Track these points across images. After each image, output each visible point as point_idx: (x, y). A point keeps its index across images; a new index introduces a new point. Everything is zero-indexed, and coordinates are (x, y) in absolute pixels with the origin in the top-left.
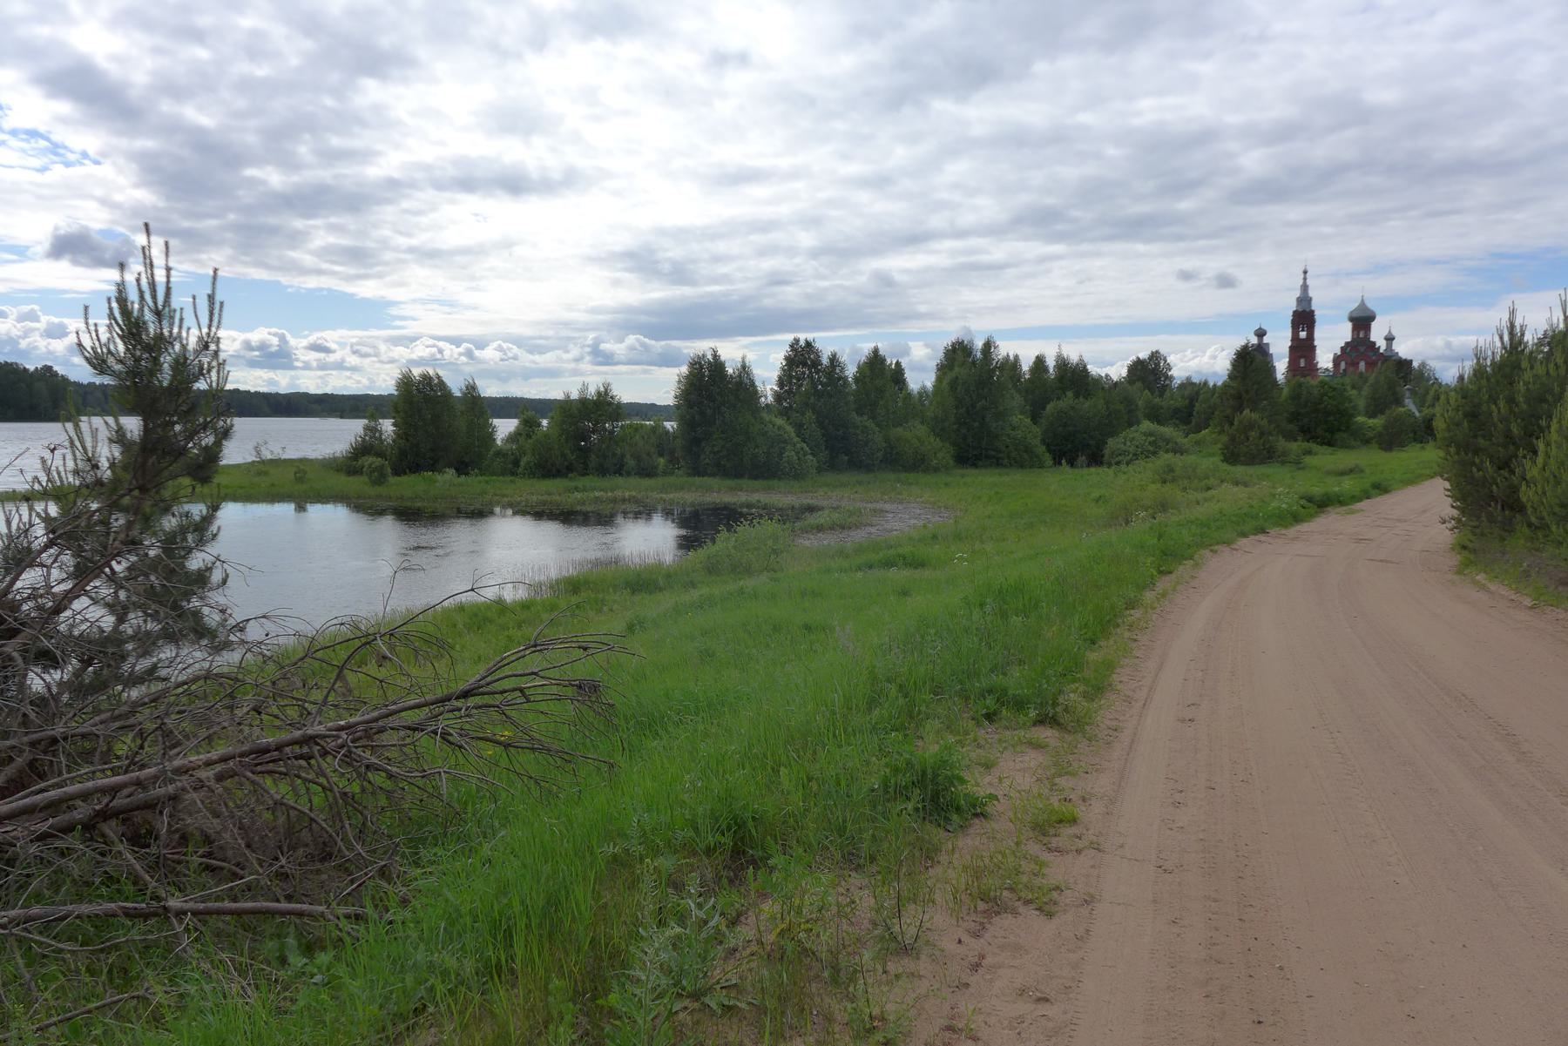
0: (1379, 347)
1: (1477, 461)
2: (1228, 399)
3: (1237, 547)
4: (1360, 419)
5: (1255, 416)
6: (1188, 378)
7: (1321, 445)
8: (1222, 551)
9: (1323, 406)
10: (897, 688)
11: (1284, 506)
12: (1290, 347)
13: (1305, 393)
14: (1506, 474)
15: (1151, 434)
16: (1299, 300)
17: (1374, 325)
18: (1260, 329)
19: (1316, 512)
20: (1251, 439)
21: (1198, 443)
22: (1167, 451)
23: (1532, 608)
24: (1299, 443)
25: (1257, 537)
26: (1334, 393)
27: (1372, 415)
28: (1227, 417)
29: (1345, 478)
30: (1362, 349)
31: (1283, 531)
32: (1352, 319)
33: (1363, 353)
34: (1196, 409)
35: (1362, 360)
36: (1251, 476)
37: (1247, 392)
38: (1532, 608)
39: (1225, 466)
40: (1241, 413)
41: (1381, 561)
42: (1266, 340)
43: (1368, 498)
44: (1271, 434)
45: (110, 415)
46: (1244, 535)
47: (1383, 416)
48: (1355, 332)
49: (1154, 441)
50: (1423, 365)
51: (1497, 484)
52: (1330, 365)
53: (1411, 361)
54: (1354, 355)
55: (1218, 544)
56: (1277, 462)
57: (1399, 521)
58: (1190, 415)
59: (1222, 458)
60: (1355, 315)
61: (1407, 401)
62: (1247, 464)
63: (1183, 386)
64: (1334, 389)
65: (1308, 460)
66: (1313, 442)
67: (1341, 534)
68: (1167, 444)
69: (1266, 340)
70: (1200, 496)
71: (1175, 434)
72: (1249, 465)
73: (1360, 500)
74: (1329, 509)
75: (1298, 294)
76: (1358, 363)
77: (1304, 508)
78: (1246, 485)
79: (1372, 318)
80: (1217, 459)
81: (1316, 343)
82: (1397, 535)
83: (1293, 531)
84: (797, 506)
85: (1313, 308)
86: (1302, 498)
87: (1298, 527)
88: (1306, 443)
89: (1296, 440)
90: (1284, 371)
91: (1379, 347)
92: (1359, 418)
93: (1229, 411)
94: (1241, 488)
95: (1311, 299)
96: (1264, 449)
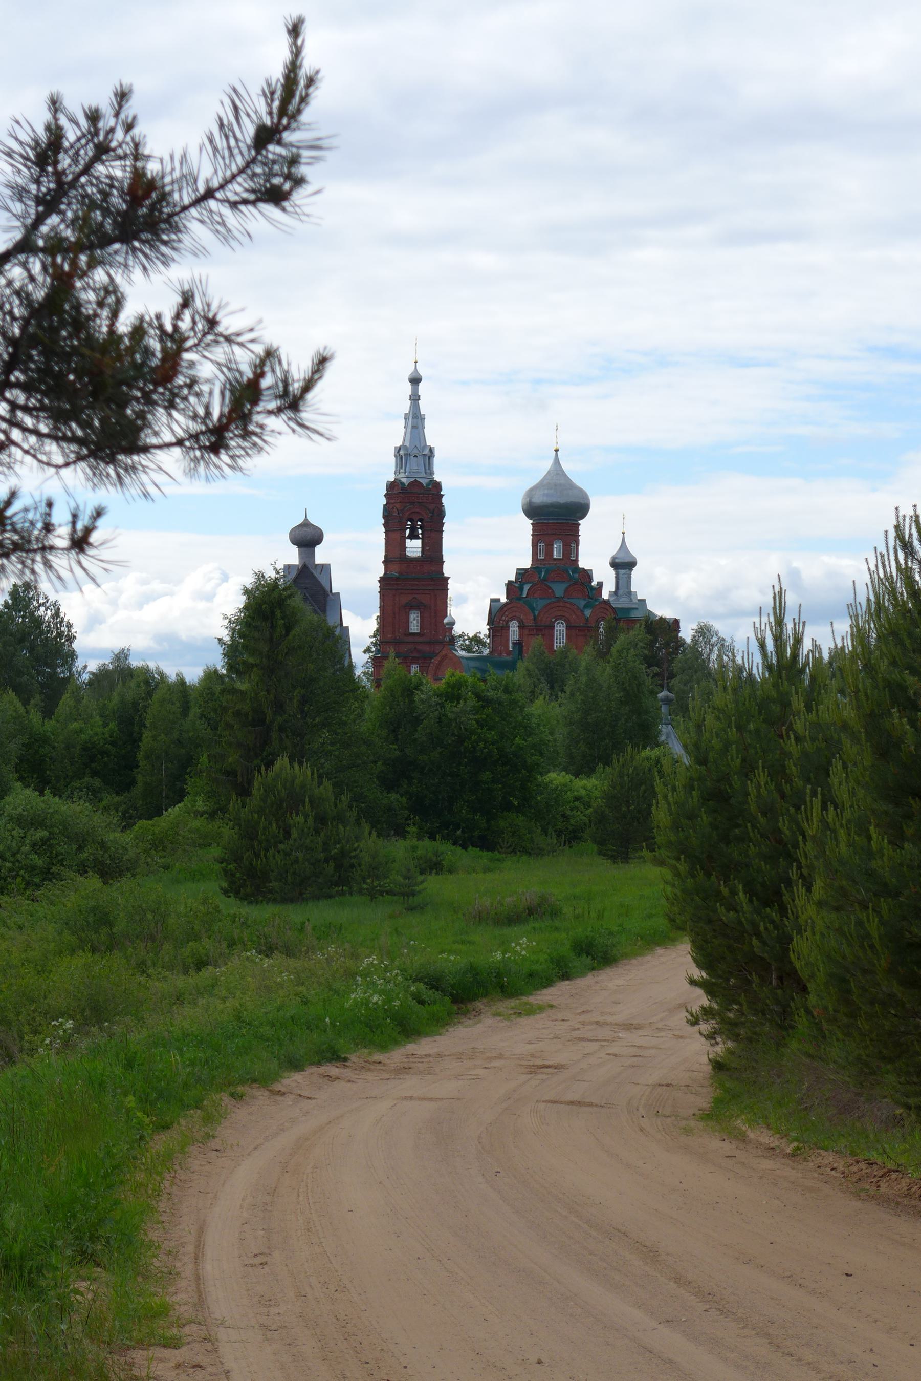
0: (600, 584)
1: (725, 891)
2: (229, 726)
3: (283, 1090)
4: (556, 778)
5: (302, 773)
6: (121, 656)
8: (254, 1098)
10: (521, 745)
11: (375, 998)
12: (382, 580)
14: (775, 916)
15: (37, 822)
16: (403, 456)
17: (586, 527)
18: (306, 524)
19: (449, 1014)
20: (295, 834)
21: (158, 844)
22: (83, 870)
23: (792, 1155)
24: (408, 843)
25: (322, 1070)
27: (583, 768)
28: (230, 773)
29: (516, 930)
30: (559, 589)
31: (377, 1057)
32: (531, 511)
33: (559, 599)
35: (512, 619)
36: (302, 929)
37: (279, 707)
38: (792, 1155)
39: (231, 906)
40: (269, 764)
41: (572, 1103)
42: (321, 555)
46: (295, 1065)
47: (608, 769)
48: (541, 545)
49: (44, 841)
50: (704, 632)
51: (758, 935)
52: (482, 629)
53: (676, 622)
54: (540, 604)
55: (242, 1082)
56: (361, 892)
57: (629, 1027)
58: (129, 763)
59: (225, 885)
60: (539, 499)
61: (665, 729)
62: (286, 900)
63: (102, 678)
65: (432, 884)
66: (445, 838)
67: (500, 1057)
68: (80, 848)
69: (321, 555)
70: (181, 982)
71: (99, 819)
72: (292, 901)
73: (548, 983)
74: (479, 1004)
75: (397, 435)
76: (552, 628)
77: (421, 1002)
78: (289, 952)
79: (580, 509)
80: (212, 887)
82: (615, 1055)
83: (396, 1056)
84: (496, 852)
85: (437, 477)
86: (417, 979)
87: (411, 1048)
88: (427, 842)
89: (401, 832)
90: (369, 641)
91: (600, 584)
92: (552, 775)
93: (233, 758)
94: (278, 958)
95: (430, 454)
96: (326, 861)
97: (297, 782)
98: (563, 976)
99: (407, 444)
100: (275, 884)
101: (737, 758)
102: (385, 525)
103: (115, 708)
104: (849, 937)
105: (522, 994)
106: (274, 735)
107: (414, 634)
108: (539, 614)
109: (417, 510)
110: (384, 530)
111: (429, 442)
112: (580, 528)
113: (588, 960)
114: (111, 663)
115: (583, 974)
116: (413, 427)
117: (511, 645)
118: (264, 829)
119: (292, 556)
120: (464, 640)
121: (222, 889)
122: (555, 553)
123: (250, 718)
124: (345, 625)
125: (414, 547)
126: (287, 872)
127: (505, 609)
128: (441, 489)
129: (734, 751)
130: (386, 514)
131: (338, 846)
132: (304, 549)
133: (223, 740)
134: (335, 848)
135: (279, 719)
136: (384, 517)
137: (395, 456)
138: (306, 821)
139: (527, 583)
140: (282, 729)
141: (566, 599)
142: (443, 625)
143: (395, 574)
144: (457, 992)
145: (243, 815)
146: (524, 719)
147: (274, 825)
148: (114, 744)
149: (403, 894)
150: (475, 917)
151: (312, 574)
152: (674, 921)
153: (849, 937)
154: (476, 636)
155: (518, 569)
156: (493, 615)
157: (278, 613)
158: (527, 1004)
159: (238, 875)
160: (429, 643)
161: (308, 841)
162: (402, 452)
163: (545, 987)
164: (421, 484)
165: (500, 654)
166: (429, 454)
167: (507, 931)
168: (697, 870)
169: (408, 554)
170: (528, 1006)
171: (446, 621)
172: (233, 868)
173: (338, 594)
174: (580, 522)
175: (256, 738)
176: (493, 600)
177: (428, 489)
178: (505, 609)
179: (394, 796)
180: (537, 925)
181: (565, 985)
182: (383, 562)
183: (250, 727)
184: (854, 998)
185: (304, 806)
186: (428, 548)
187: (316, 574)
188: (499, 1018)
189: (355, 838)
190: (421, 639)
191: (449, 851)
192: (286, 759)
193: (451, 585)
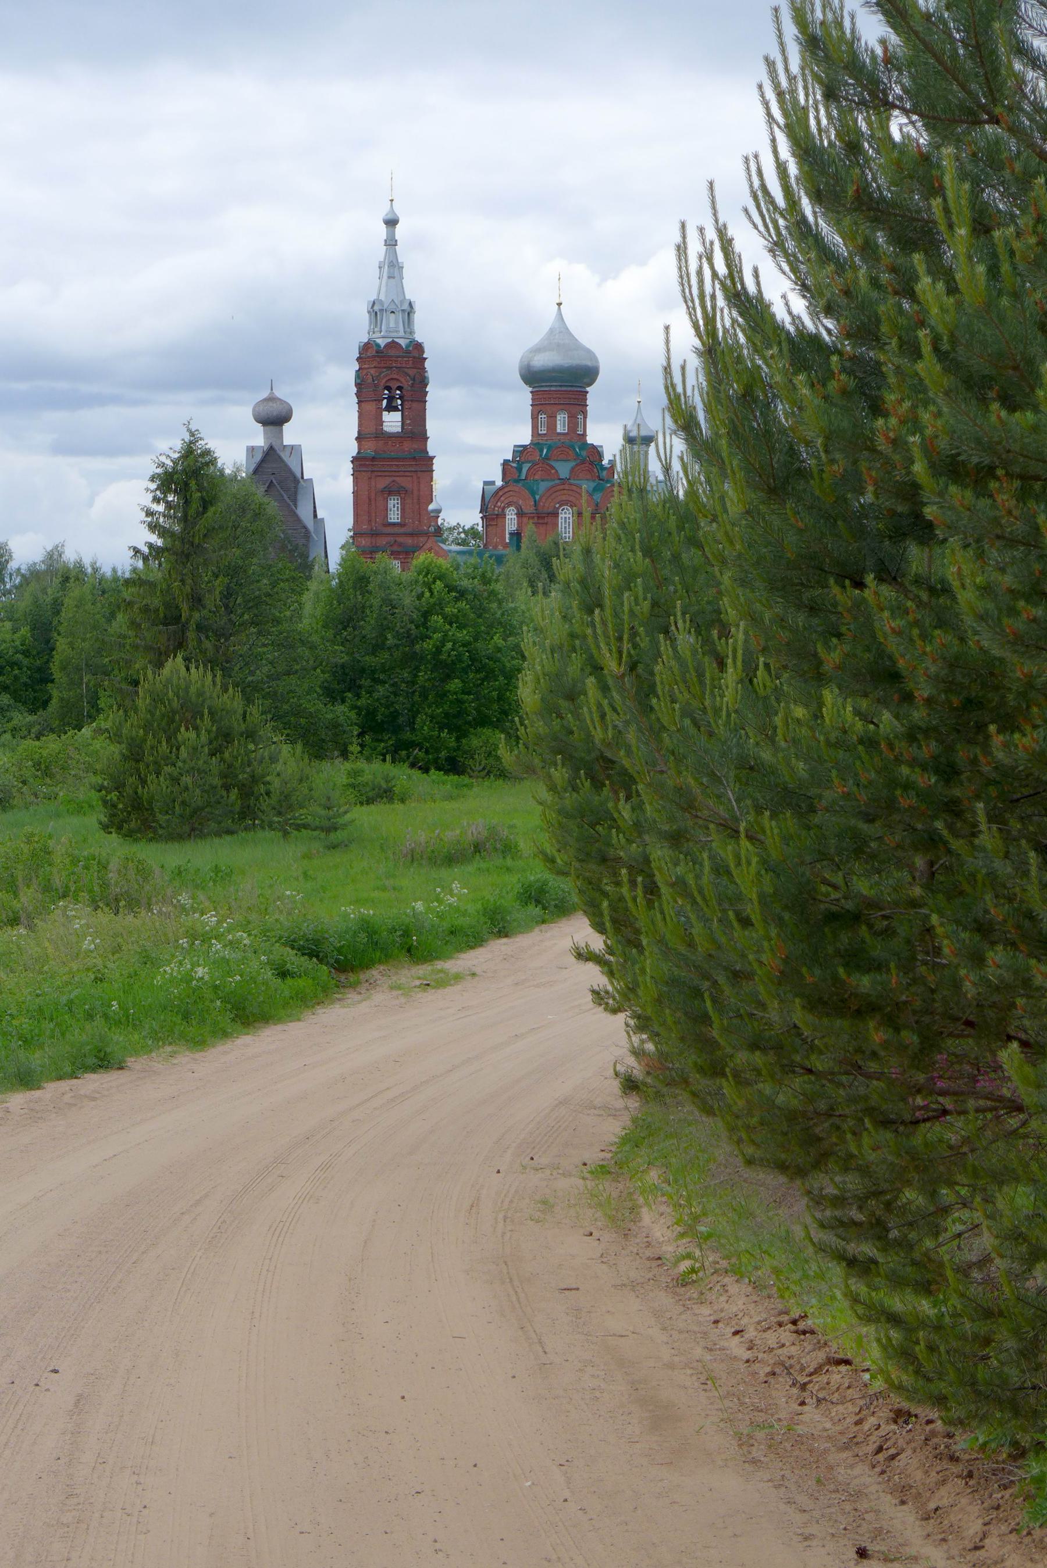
7: (426, 770)
9: (428, 645)
11: (200, 971)
13: (376, 602)
16: (376, 312)
17: (594, 394)
18: (271, 399)
24: (348, 766)
26: (462, 604)
30: (563, 469)
32: (532, 377)
33: (564, 481)
34: (57, 657)
35: (509, 505)
37: (197, 601)
43: (503, 933)
44: (250, 735)
45: (298, 520)
48: (542, 417)
58: (43, 677)
59: (105, 820)
62: (178, 837)
64: (462, 594)
69: (290, 435)
73: (472, 939)
74: (374, 973)
76: (555, 514)
81: (432, 448)
85: (419, 337)
97: (193, 690)
98: (499, 932)
99: (382, 297)
100: (162, 818)
101: (645, 599)
102: (358, 394)
103: (27, 610)
104: (699, 899)
105: (438, 958)
106: (191, 635)
107: (394, 524)
108: (541, 498)
109: (395, 376)
110: (356, 400)
111: (409, 296)
112: (588, 396)
113: (537, 911)
114: (43, 562)
115: (526, 927)
116: (389, 277)
117: (507, 536)
118: (152, 748)
119: (258, 438)
120: (459, 533)
121: (100, 823)
122: (558, 426)
123: (162, 615)
124: (319, 516)
125: (392, 421)
126: (174, 801)
127: (501, 493)
128: (423, 352)
129: (640, 589)
130: (359, 381)
131: (248, 770)
132: (269, 428)
133: (128, 641)
134: (245, 772)
135: (196, 615)
136: (357, 385)
137: (369, 312)
138: (198, 736)
139: (527, 462)
140: (199, 628)
141: (572, 481)
142: (428, 513)
143: (370, 453)
144: (346, 957)
145: (124, 731)
146: (503, 614)
147: (164, 743)
148: (26, 653)
149: (322, 829)
150: (405, 856)
151: (280, 457)
152: (553, 861)
153: (699, 899)
154: (472, 528)
155: (515, 446)
156: (487, 500)
157: (193, 484)
158: (441, 971)
159: (121, 806)
160: (412, 535)
161: (201, 762)
162: (376, 308)
163: (472, 948)
164: (400, 345)
165: (495, 547)
166: (409, 309)
167: (444, 873)
168: (580, 778)
169: (385, 429)
170: (442, 975)
171: (431, 507)
172: (115, 798)
173: (311, 480)
174: (588, 389)
175: (169, 640)
176: (486, 483)
177: (408, 352)
178: (501, 493)
179: (340, 709)
180: (483, 865)
181: (499, 947)
182: (357, 439)
183: (161, 627)
184: (715, 1033)
185: (202, 719)
186: (408, 422)
187: (285, 456)
188: (395, 993)
189: (270, 758)
190: (402, 530)
191: (403, 775)
192: (179, 659)
193: (437, 464)
